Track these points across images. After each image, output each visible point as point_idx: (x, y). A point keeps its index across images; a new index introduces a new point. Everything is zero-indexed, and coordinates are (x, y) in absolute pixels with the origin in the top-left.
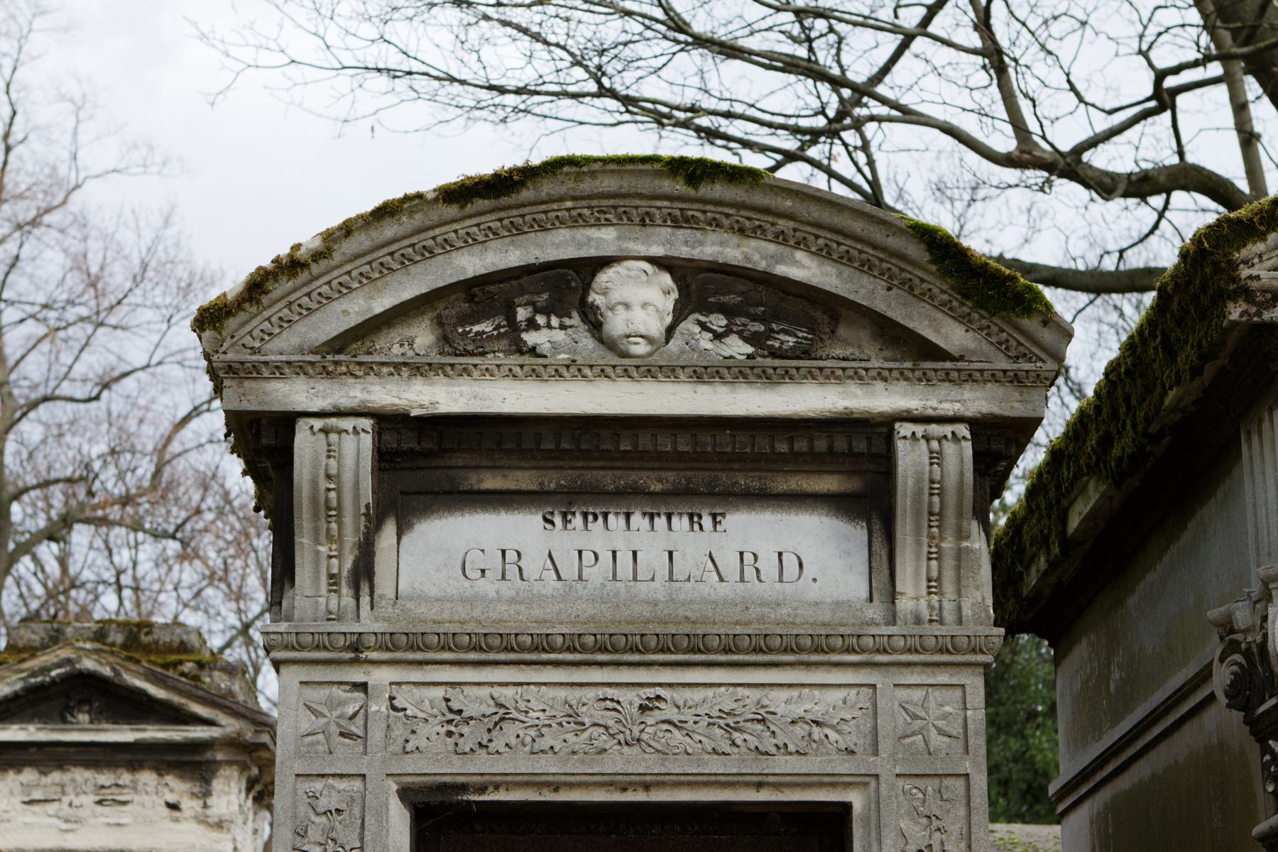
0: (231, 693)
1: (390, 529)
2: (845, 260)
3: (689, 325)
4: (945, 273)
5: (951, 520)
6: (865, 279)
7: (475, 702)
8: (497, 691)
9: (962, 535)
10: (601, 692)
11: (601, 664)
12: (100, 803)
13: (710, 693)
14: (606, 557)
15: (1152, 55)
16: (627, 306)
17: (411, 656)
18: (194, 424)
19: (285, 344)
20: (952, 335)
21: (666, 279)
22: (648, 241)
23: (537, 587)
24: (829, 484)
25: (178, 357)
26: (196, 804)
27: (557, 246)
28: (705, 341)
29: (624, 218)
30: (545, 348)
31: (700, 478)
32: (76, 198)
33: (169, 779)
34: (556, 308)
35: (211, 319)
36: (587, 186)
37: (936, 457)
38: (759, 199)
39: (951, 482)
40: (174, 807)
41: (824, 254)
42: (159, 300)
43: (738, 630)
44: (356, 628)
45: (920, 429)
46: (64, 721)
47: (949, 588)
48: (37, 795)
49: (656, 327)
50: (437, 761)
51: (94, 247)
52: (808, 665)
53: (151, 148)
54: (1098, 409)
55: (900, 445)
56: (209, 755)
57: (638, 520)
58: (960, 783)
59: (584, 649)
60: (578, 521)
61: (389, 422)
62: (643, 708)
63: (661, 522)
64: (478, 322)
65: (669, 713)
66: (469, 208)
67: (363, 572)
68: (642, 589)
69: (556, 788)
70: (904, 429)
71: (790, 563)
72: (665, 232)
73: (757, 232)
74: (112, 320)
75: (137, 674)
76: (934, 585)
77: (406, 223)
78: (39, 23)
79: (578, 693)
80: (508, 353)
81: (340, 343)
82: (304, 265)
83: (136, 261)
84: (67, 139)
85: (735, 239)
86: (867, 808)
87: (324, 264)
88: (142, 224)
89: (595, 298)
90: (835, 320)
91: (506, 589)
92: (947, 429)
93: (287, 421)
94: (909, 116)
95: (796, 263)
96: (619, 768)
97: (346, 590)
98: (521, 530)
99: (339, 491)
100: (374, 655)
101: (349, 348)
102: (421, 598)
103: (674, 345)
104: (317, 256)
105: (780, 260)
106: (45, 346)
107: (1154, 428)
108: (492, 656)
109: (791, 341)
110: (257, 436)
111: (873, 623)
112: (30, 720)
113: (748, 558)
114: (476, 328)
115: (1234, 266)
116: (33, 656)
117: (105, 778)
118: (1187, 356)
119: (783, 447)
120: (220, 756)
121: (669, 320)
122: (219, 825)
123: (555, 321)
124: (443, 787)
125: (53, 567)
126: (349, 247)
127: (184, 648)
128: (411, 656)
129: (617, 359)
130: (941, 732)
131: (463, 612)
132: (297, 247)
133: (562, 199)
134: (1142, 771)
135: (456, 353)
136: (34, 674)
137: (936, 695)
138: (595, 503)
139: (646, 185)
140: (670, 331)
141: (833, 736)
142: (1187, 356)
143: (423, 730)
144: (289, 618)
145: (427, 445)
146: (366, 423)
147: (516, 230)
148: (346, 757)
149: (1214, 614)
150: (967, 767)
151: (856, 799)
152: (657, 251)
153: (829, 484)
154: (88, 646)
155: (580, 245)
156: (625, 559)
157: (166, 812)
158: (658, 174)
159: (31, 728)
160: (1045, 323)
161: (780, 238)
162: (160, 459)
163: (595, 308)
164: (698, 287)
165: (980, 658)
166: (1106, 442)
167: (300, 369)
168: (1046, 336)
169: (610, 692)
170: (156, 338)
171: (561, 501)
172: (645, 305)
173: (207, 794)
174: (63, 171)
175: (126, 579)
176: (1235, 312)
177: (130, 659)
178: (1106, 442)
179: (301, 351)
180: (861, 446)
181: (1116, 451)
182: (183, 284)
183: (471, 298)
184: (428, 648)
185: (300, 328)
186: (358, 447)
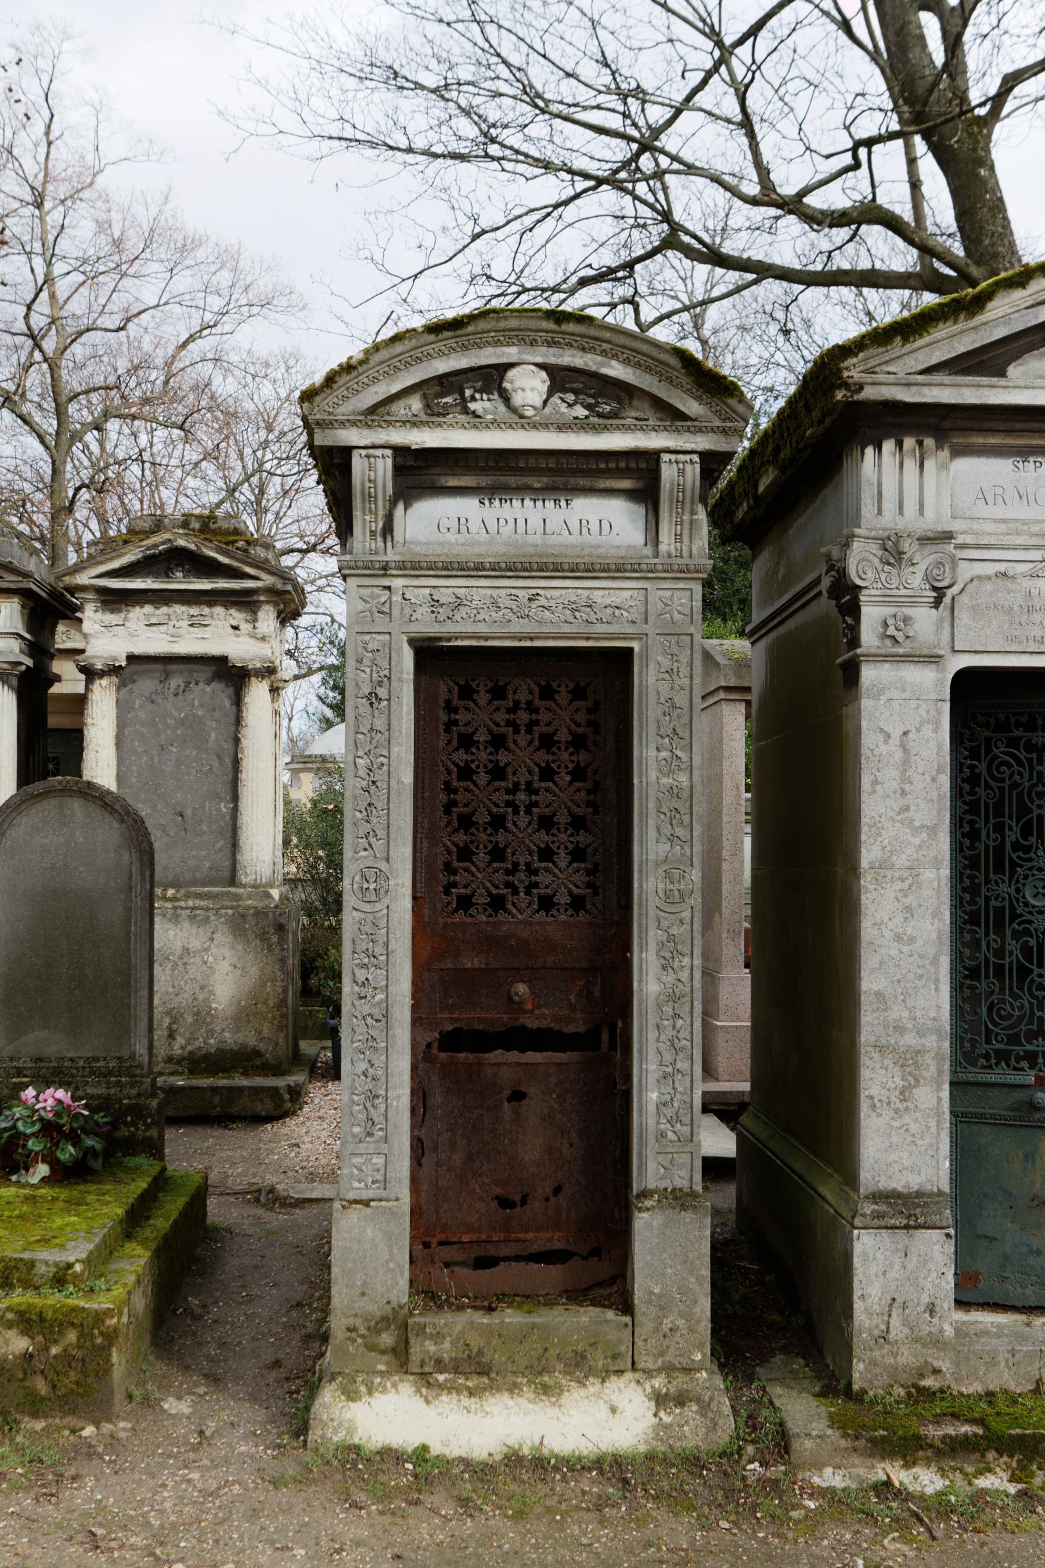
0: (267, 560)
1: (401, 506)
2: (638, 365)
3: (555, 399)
4: (689, 374)
5: (688, 505)
6: (648, 376)
7: (445, 596)
8: (456, 591)
9: (693, 512)
10: (509, 591)
11: (509, 577)
12: (191, 625)
13: (564, 592)
14: (511, 522)
15: (852, 129)
16: (523, 390)
17: (413, 573)
18: (191, 346)
19: (346, 409)
20: (692, 407)
21: (544, 374)
22: (534, 354)
23: (476, 537)
24: (626, 484)
25: (177, 300)
26: (250, 626)
27: (487, 357)
28: (563, 408)
29: (522, 341)
30: (480, 412)
31: (559, 481)
32: (99, 179)
33: (232, 611)
34: (486, 389)
35: (308, 396)
36: (502, 324)
37: (682, 472)
38: (593, 332)
39: (689, 486)
40: (235, 628)
41: (627, 362)
42: (162, 256)
43: (579, 560)
44: (385, 559)
45: (673, 457)
46: (168, 577)
47: (686, 539)
48: (154, 621)
49: (538, 402)
50: (426, 625)
51: (115, 216)
52: (613, 578)
53: (151, 141)
54: (774, 432)
55: (663, 466)
56: (255, 598)
57: (528, 502)
58: (688, 638)
59: (501, 570)
60: (497, 502)
61: (400, 452)
62: (530, 600)
63: (539, 503)
64: (445, 397)
65: (543, 602)
66: (440, 336)
67: (388, 529)
68: (530, 539)
69: (486, 639)
70: (665, 457)
71: (605, 525)
72: (543, 349)
73: (592, 350)
74: (131, 271)
75: (211, 549)
76: (679, 538)
77: (407, 344)
78: (66, 46)
79: (497, 591)
80: (461, 413)
81: (372, 410)
82: (354, 368)
83: (146, 228)
84: (92, 135)
85: (580, 354)
86: (641, 650)
87: (365, 366)
88: (149, 201)
89: (506, 385)
90: (631, 397)
91: (461, 539)
92: (687, 457)
93: (347, 451)
94: (690, 169)
95: (612, 367)
96: (518, 630)
97: (379, 539)
98: (468, 507)
99: (375, 488)
100: (394, 572)
101: (376, 413)
102: (417, 543)
103: (547, 410)
104: (362, 362)
105: (603, 365)
106: (84, 291)
107: (801, 446)
108: (454, 573)
109: (608, 408)
110: (332, 458)
111: (647, 557)
112: (147, 576)
113: (584, 523)
114: (444, 400)
115: (840, 371)
116: (148, 537)
117: (194, 611)
118: (816, 414)
119: (603, 466)
120: (262, 598)
121: (545, 396)
122: (263, 639)
123: (485, 397)
124: (430, 639)
125: (95, 448)
126: (377, 357)
127: (236, 532)
128: (413, 573)
129: (519, 418)
130: (679, 612)
131: (439, 550)
132: (350, 358)
133: (489, 332)
134: (791, 624)
135: (434, 414)
136: (148, 549)
137: (678, 594)
138: (506, 494)
139: (533, 324)
140: (545, 402)
141: (625, 614)
142: (816, 414)
143: (420, 610)
144: (351, 553)
145: (419, 463)
146: (389, 452)
147: (465, 348)
148: (381, 623)
149: (823, 550)
150: (692, 630)
151: (636, 645)
152: (539, 360)
153: (626, 484)
154: (181, 531)
155: (499, 357)
156: (521, 523)
157: (231, 631)
158: (540, 318)
159: (149, 581)
160: (740, 402)
161: (604, 353)
162: (169, 371)
163: (506, 390)
164: (560, 379)
165: (700, 575)
166: (777, 450)
167: (354, 424)
168: (740, 408)
169: (513, 591)
170: (163, 286)
171: (489, 492)
172: (532, 389)
173: (255, 620)
174: (90, 158)
175: (146, 456)
176: (840, 395)
177: (206, 539)
178: (777, 450)
179: (354, 413)
180: (643, 465)
181: (782, 456)
182: (179, 245)
183: (441, 384)
184: (421, 568)
185: (353, 401)
186: (385, 465)
